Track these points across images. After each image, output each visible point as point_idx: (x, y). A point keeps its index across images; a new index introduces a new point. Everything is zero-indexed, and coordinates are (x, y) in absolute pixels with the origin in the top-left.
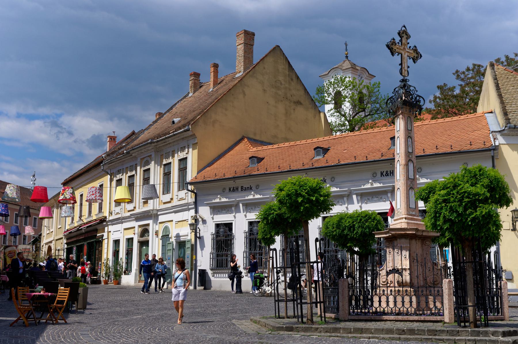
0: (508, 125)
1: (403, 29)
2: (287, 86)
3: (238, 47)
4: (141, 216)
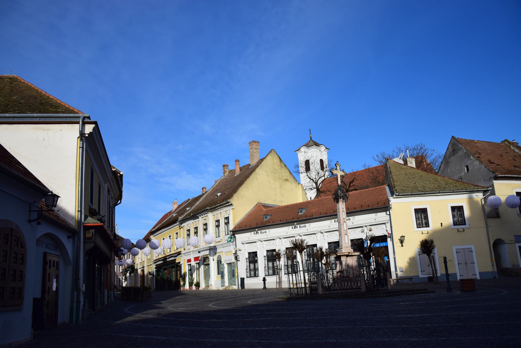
4: (112, 282)
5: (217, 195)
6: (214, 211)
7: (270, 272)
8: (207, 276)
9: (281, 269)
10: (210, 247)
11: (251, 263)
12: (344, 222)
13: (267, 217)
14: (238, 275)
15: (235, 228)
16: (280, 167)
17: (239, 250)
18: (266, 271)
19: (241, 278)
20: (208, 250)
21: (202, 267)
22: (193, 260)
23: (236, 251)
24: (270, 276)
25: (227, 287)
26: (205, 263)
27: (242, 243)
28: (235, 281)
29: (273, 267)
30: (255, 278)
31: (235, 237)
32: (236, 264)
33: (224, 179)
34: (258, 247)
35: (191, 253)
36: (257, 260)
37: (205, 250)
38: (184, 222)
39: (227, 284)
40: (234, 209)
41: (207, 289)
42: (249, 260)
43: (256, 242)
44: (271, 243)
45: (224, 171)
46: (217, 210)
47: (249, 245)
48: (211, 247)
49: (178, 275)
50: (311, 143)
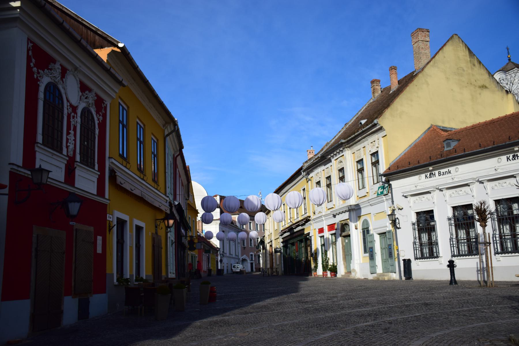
2: (470, 71)
3: (414, 46)
5: (361, 123)
6: (353, 146)
7: (463, 250)
8: (349, 255)
9: (490, 243)
10: (349, 207)
11: (422, 233)
13: (450, 143)
14: (398, 254)
15: (389, 169)
16: (469, 65)
17: (399, 209)
18: (453, 247)
19: (404, 260)
20: (346, 211)
21: (340, 239)
22: (326, 229)
23: (394, 210)
24: (462, 257)
25: (380, 275)
26: (344, 234)
27: (403, 196)
28: (393, 265)
29: (468, 239)
30: (431, 259)
31: (390, 185)
32: (394, 235)
33: (373, 102)
34: (435, 201)
35: (323, 218)
36: (434, 225)
37: (343, 212)
38: (312, 171)
39: (380, 270)
40: (386, 135)
41: (348, 278)
42: (418, 226)
43: (430, 193)
44: (460, 192)
45: (374, 89)
46: (359, 143)
47: (418, 199)
48: (351, 206)
49: (309, 252)
50: (511, 65)
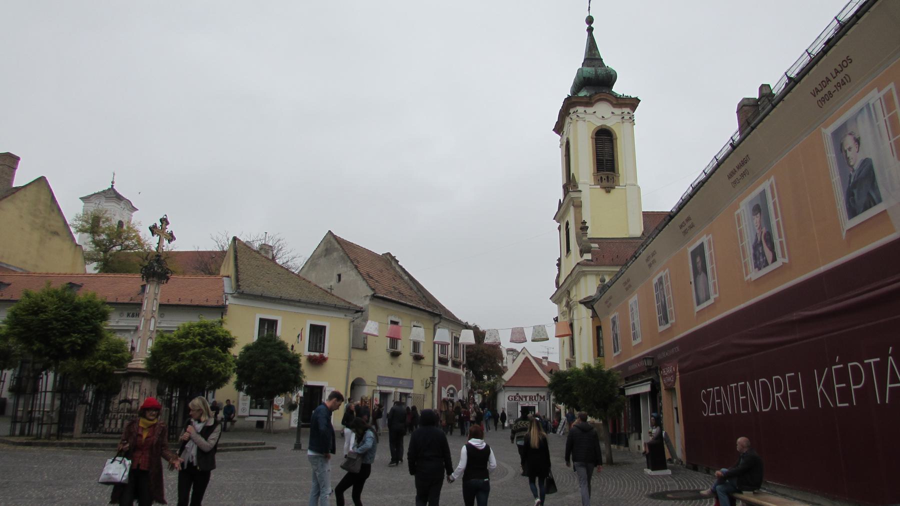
0: (238, 290)
1: (165, 217)
12: (153, 317)
